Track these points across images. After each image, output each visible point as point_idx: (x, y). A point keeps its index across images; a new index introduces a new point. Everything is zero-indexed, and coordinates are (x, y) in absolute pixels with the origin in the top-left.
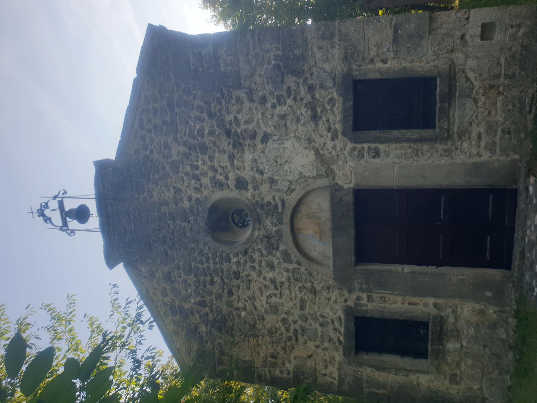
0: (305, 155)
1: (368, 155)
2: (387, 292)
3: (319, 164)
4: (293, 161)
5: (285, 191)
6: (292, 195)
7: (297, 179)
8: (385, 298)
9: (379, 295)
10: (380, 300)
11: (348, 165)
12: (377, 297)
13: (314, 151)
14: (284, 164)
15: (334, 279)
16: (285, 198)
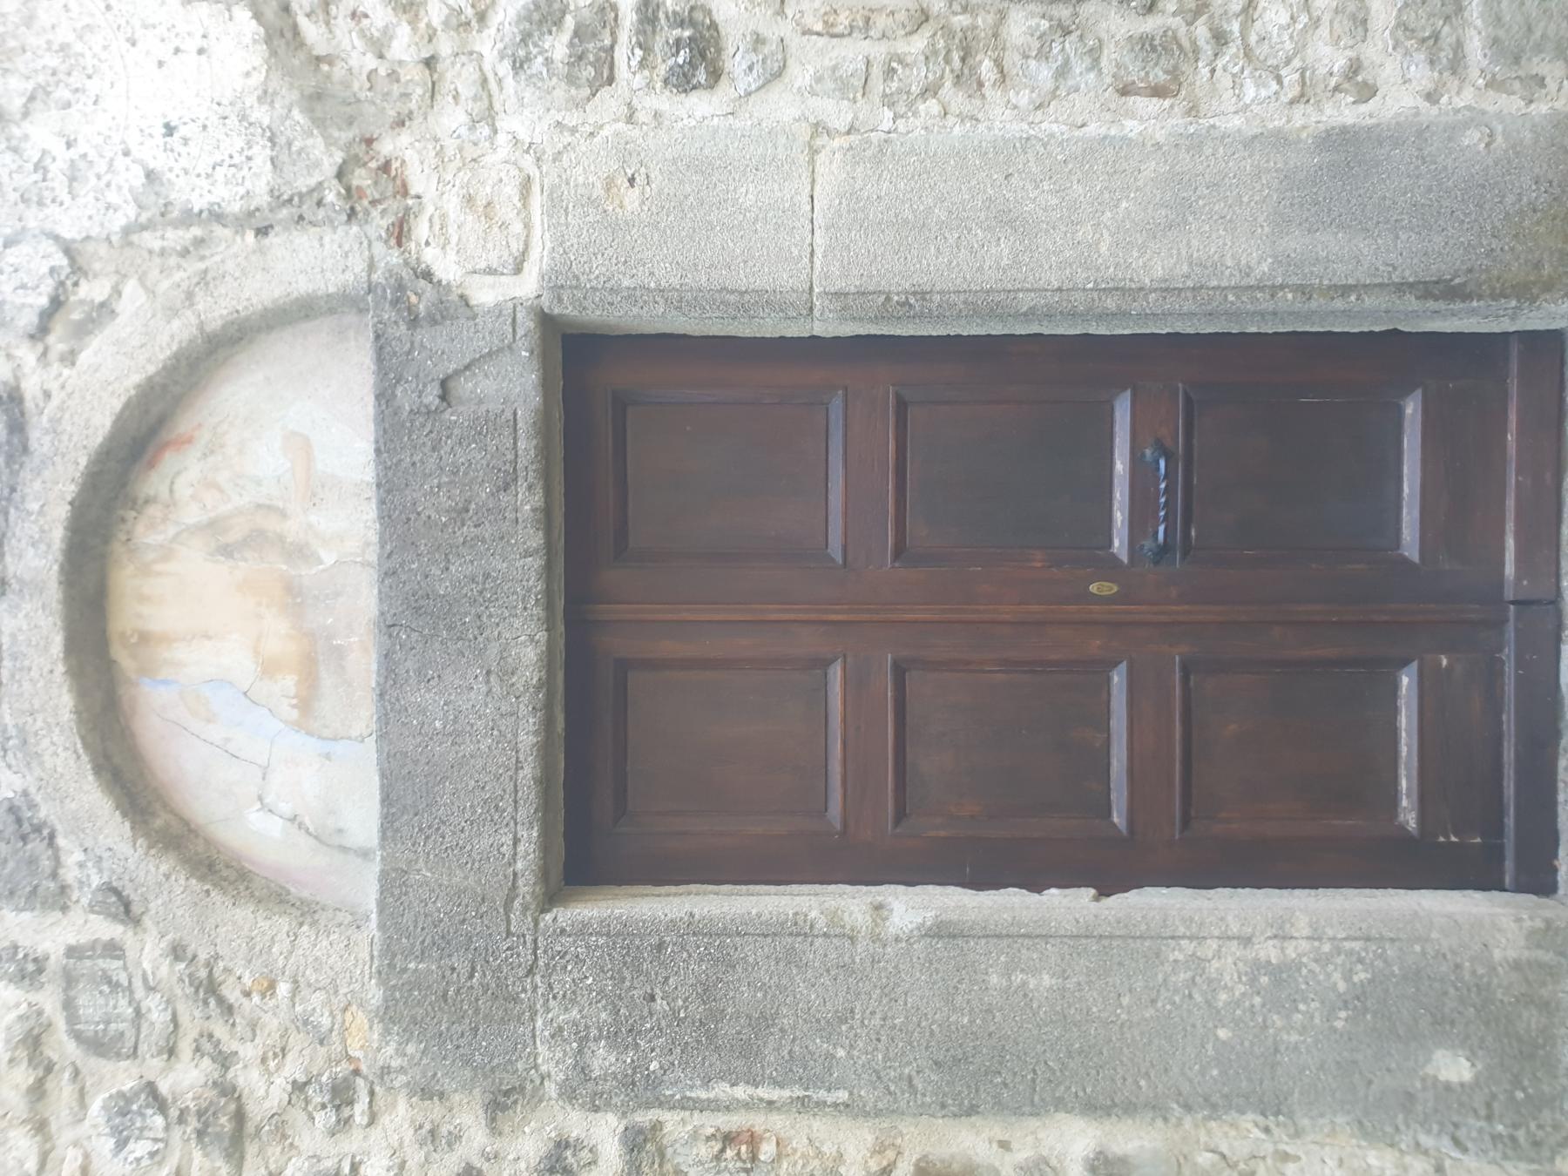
0: (191, 45)
1: (643, 64)
2: (764, 1092)
3: (296, 114)
4: (93, 86)
5: (29, 319)
6: (85, 358)
7: (127, 231)
8: (753, 1140)
9: (712, 1122)
10: (718, 1157)
11: (502, 138)
12: (695, 1135)
13: (258, 16)
14: (26, 114)
15: (388, 1015)
16: (31, 387)
